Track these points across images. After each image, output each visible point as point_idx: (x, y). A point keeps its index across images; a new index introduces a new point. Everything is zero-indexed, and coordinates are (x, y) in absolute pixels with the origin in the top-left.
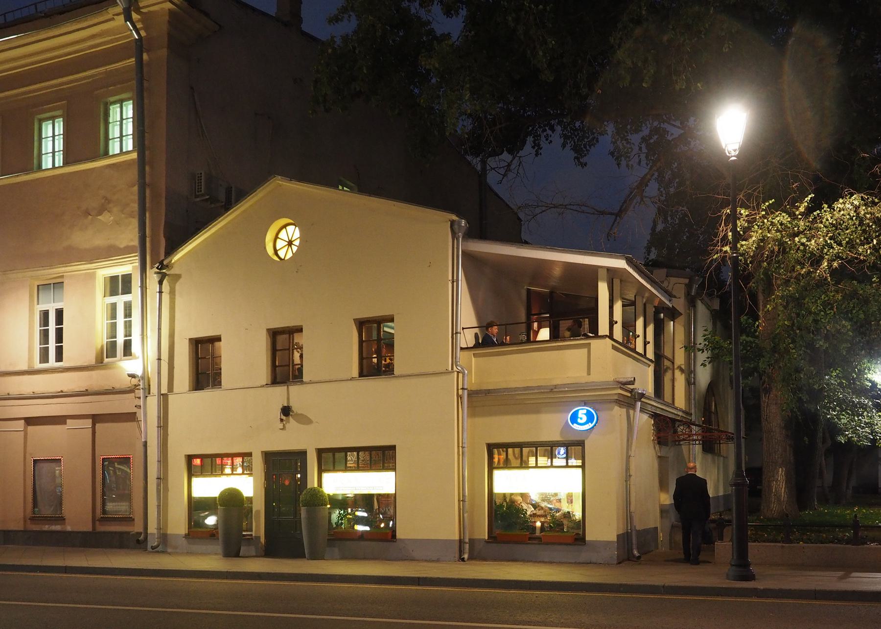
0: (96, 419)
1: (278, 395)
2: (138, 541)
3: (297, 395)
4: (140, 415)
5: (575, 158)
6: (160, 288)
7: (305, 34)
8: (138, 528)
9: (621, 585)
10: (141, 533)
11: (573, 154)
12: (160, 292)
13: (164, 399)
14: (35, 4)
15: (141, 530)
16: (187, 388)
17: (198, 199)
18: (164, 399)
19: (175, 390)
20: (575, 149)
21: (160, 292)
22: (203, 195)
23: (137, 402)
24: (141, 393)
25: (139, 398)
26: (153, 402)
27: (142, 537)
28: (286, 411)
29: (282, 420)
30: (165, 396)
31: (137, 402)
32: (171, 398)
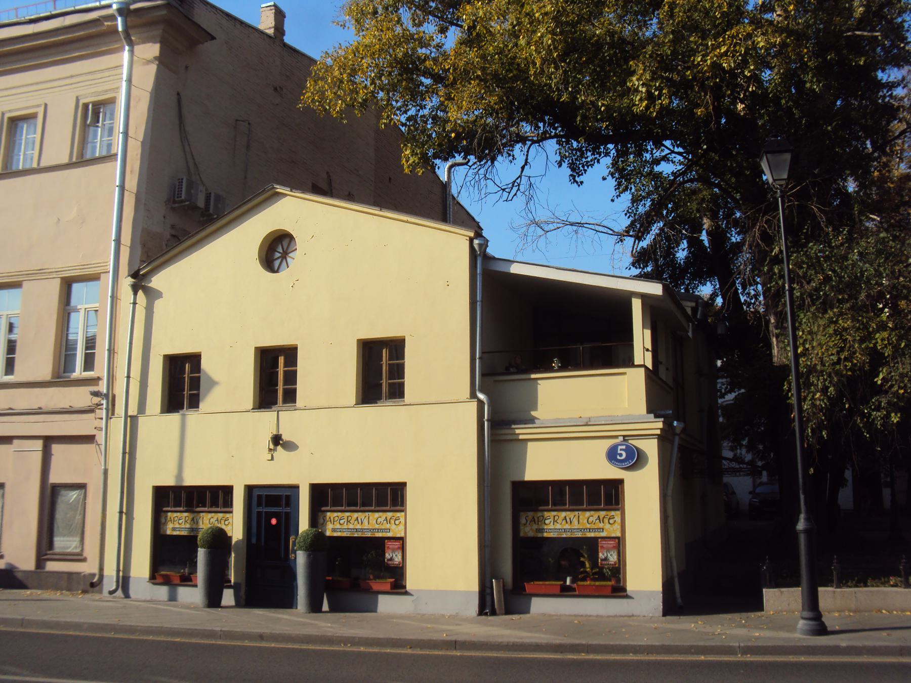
0: (49, 441)
1: (267, 418)
2: (92, 585)
3: (288, 421)
4: (100, 437)
5: (571, 175)
6: (135, 299)
7: (286, 46)
8: (88, 568)
9: (692, 647)
10: (94, 575)
11: (569, 172)
12: (135, 303)
13: (132, 423)
14: (16, 9)
15: (95, 570)
16: (250, 405)
17: (176, 205)
18: (132, 423)
19: (148, 412)
20: (573, 167)
21: (135, 303)
22: (182, 201)
23: (97, 423)
24: (103, 414)
25: (102, 419)
26: (118, 425)
27: (95, 580)
28: (277, 440)
29: (270, 450)
30: (134, 419)
31: (97, 423)
32: (141, 420)
